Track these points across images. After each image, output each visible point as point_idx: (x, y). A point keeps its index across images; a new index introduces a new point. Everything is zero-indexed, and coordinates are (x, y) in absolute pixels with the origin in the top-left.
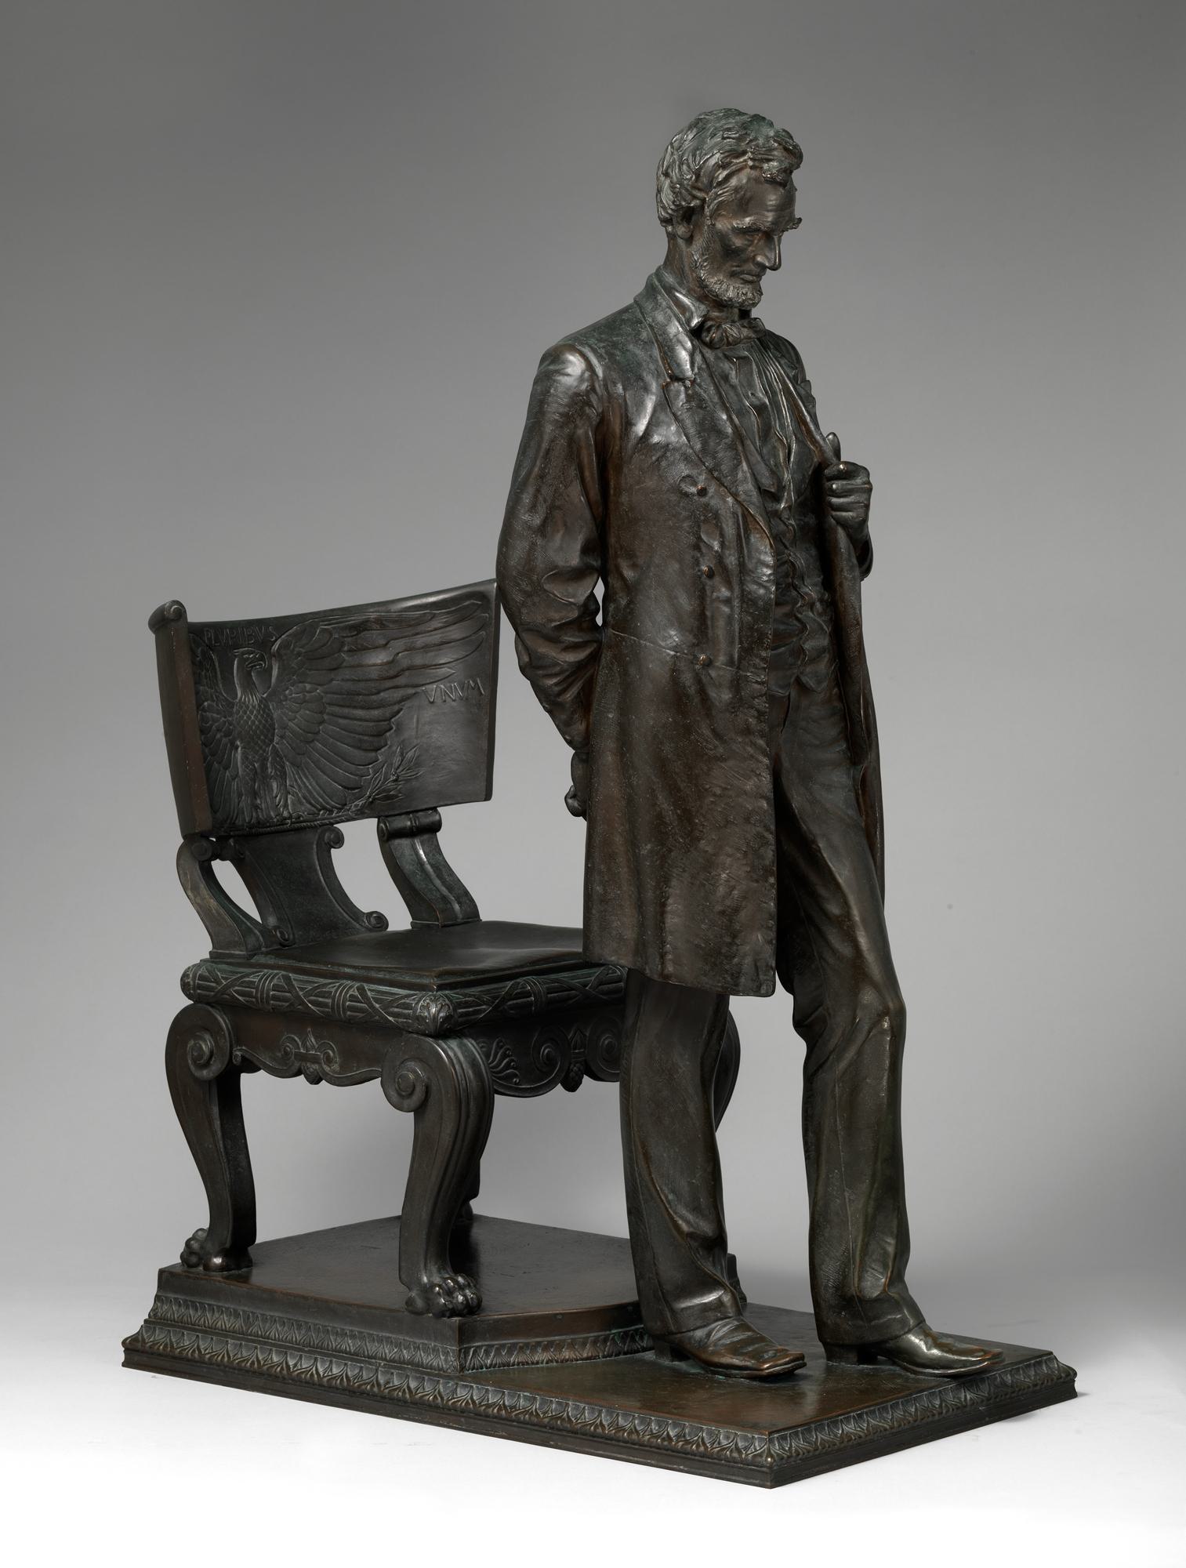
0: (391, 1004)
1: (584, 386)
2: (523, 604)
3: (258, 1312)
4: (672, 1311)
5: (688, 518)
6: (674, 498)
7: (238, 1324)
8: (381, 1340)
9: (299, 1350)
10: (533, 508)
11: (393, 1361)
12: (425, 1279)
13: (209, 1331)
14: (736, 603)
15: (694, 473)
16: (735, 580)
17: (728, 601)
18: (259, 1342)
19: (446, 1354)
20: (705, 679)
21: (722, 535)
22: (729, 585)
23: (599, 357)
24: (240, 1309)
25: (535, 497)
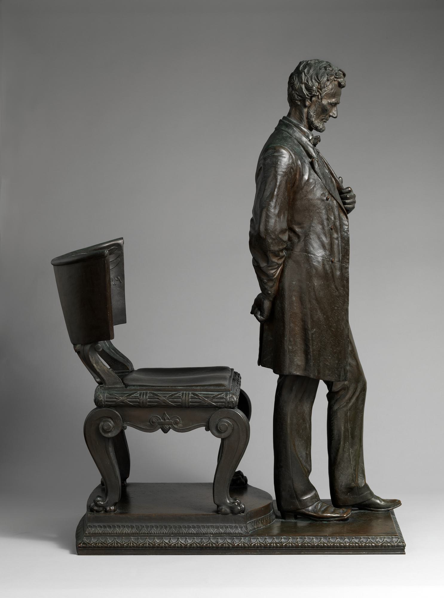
0: (214, 397)
1: (291, 161)
2: (272, 243)
3: (143, 524)
4: (300, 501)
5: (324, 209)
6: (319, 202)
7: (134, 531)
8: (208, 527)
9: (168, 536)
10: (275, 207)
11: (216, 534)
12: (228, 501)
13: (120, 535)
14: (340, 239)
15: (324, 192)
16: (339, 231)
17: (337, 239)
18: (147, 536)
19: (241, 528)
20: (333, 267)
21: (334, 215)
22: (337, 232)
23: (291, 150)
24: (134, 525)
25: (276, 203)
